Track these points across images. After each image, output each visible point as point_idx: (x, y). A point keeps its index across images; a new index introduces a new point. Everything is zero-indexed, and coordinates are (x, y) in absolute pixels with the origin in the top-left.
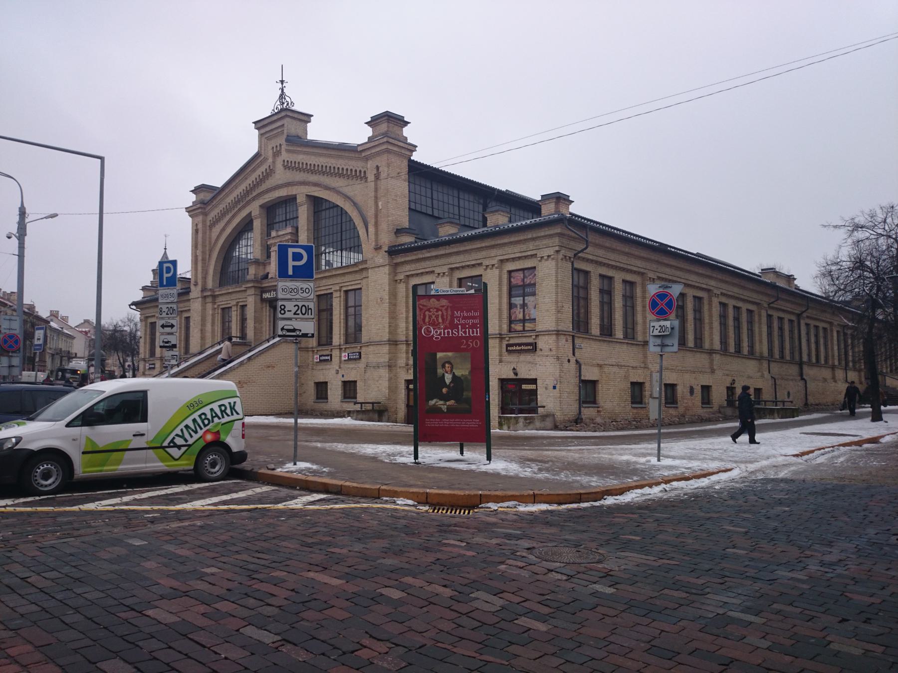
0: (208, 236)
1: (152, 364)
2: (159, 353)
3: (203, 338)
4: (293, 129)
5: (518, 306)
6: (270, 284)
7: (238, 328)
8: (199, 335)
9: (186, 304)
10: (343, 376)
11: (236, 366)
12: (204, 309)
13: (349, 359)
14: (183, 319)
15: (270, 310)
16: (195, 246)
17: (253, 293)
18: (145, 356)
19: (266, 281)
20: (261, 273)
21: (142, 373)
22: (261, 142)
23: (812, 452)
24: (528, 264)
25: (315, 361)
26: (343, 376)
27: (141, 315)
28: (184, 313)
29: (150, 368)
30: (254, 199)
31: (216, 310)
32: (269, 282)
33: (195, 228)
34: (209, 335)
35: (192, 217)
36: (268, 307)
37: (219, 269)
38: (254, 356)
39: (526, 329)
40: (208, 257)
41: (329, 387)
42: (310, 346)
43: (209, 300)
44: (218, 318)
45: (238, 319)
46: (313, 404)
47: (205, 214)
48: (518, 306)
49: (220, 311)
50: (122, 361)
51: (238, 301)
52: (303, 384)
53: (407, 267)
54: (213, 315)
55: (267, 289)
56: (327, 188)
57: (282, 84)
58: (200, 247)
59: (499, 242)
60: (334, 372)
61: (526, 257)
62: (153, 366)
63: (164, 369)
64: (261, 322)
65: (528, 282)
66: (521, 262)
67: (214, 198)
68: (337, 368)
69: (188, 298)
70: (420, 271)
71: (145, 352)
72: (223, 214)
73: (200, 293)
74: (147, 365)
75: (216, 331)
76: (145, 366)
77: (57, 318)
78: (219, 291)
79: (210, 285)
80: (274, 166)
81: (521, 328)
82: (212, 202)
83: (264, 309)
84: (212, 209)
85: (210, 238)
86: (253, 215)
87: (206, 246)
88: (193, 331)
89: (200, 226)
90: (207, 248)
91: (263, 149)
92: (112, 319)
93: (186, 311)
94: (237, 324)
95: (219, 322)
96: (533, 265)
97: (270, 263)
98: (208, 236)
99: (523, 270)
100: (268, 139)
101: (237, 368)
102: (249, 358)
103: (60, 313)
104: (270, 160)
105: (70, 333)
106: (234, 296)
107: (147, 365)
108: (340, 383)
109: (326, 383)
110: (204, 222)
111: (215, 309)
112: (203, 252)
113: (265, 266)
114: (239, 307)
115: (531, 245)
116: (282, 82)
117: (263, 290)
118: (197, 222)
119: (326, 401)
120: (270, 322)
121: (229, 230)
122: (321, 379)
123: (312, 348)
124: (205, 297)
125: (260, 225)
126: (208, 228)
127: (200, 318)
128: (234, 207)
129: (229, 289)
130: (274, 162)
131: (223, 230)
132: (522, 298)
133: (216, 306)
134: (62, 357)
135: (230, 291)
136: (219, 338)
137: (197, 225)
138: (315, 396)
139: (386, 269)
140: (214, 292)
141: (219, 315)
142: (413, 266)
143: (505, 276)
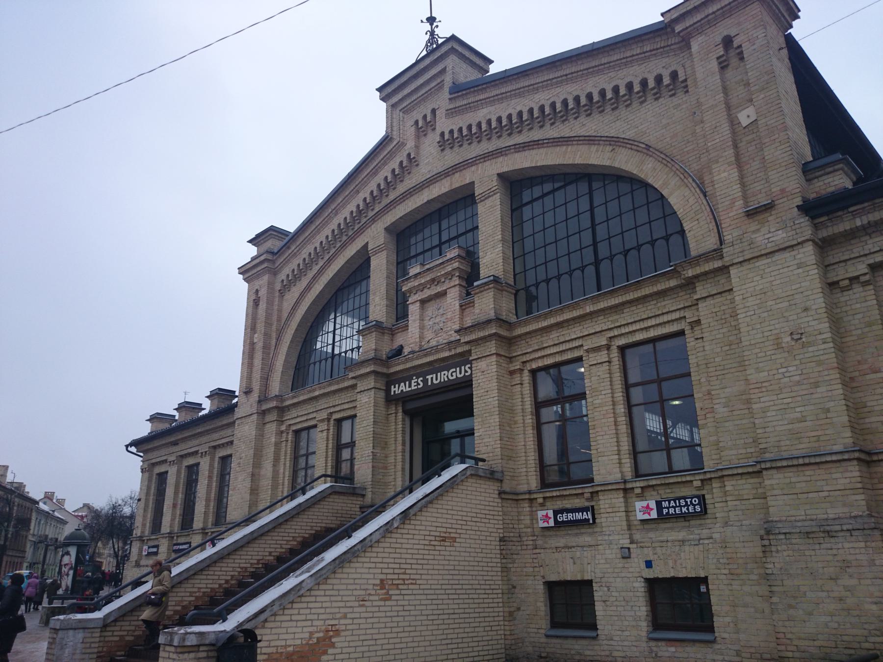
0: (276, 308)
1: (153, 547)
2: (168, 525)
3: (254, 491)
4: (462, 75)
6: (409, 365)
7: (329, 464)
8: (248, 484)
9: (228, 432)
11: (375, 537)
12: (260, 435)
13: (662, 517)
14: (217, 459)
15: (403, 420)
16: (251, 327)
17: (372, 385)
18: (143, 532)
19: (401, 359)
20: (386, 349)
21: (134, 564)
22: (392, 118)
25: (542, 524)
26: (649, 564)
27: (143, 461)
28: (218, 450)
29: (149, 554)
30: (374, 220)
31: (284, 435)
32: (407, 361)
33: (254, 297)
34: (266, 483)
35: (247, 282)
36: (400, 415)
37: (294, 359)
38: (415, 509)
40: (273, 342)
41: (597, 595)
42: (524, 488)
43: (273, 416)
44: (287, 449)
45: (330, 446)
46: (544, 640)
47: (275, 273)
49: (290, 437)
50: (116, 550)
51: (332, 410)
52: (514, 587)
54: (277, 445)
55: (400, 376)
56: (590, 140)
57: (431, 24)
58: (261, 327)
60: (612, 554)
62: (155, 550)
63: (173, 556)
64: (385, 446)
67: (286, 246)
68: (626, 542)
69: (231, 420)
71: (144, 525)
72: (307, 265)
73: (255, 405)
74: (145, 547)
75: (281, 476)
76: (141, 550)
77: (52, 500)
78: (294, 397)
79: (275, 388)
80: (418, 153)
82: (289, 248)
83: (392, 418)
84: (287, 261)
85: (280, 311)
86: (370, 247)
87: (271, 325)
88: (236, 478)
89: (263, 293)
90: (274, 328)
91: (395, 129)
92: (111, 497)
93: (223, 446)
94: (327, 457)
95: (288, 457)
97: (406, 327)
98: (276, 308)
100: (406, 111)
101: (378, 542)
102: (405, 514)
103: (55, 495)
104: (410, 144)
105: (60, 516)
106: (323, 404)
107: (145, 547)
108: (640, 586)
109: (589, 583)
110: (271, 285)
111: (282, 432)
112: (267, 335)
113: (393, 335)
114: (332, 422)
116: (431, 20)
117: (391, 380)
118: (257, 287)
119: (593, 634)
120: (404, 444)
121: (318, 287)
122: (570, 573)
123: (530, 492)
124: (263, 413)
125: (385, 262)
126: (277, 294)
127: (252, 452)
128: (329, 249)
129: (314, 390)
130: (417, 147)
131: (308, 288)
133: (283, 428)
134: (47, 546)
135: (317, 393)
136: (286, 489)
137: (257, 291)
138: (548, 617)
139: (808, 253)
140: (282, 401)
141: (289, 444)
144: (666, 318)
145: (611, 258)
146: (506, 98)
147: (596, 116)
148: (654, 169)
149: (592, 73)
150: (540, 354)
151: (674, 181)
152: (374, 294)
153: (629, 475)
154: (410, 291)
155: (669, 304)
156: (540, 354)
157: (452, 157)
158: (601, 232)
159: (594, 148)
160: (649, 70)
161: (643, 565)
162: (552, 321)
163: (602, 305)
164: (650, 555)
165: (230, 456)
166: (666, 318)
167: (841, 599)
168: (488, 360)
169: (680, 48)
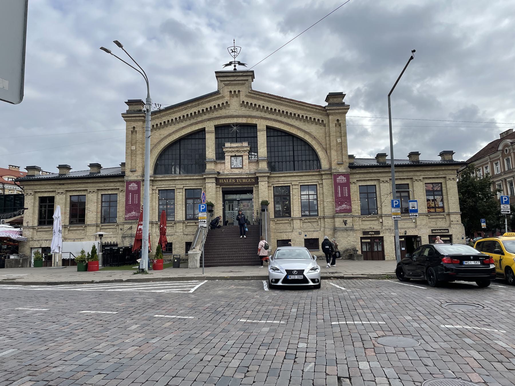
5: (431, 200)
10: (306, 236)
23: (128, 281)
24: (83, 193)
26: (306, 236)
39: (437, 211)
48: (431, 200)
53: (358, 176)
56: (299, 129)
59: (425, 169)
60: (297, 233)
61: (437, 178)
65: (436, 189)
66: (49, 193)
70: (367, 179)
81: (434, 211)
96: (116, 193)
99: (432, 183)
108: (303, 240)
115: (412, 174)
132: (433, 197)
142: (362, 176)
143: (100, 197)
144: (313, 181)
145: (298, 161)
146: (271, 102)
147: (298, 121)
148: (315, 144)
149: (300, 109)
150: (278, 183)
151: (320, 149)
152: (208, 148)
153: (184, 220)
154: (227, 151)
155: (314, 178)
156: (278, 183)
157: (244, 111)
158: (292, 153)
159: (299, 131)
160: (318, 117)
161: (304, 236)
162: (284, 175)
163: (299, 174)
164: (306, 233)
165: (310, 270)
166: (313, 181)
167: (347, 241)
168: (265, 183)
169: (325, 115)
